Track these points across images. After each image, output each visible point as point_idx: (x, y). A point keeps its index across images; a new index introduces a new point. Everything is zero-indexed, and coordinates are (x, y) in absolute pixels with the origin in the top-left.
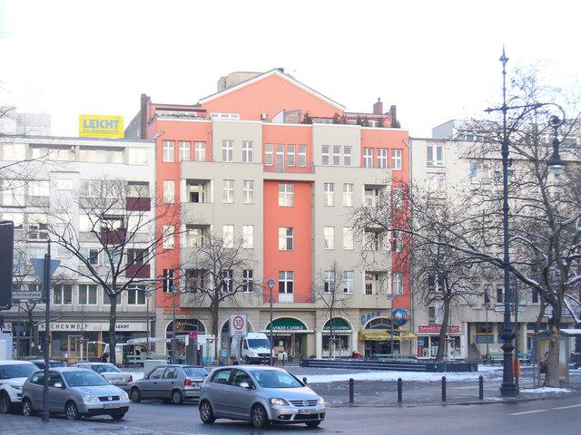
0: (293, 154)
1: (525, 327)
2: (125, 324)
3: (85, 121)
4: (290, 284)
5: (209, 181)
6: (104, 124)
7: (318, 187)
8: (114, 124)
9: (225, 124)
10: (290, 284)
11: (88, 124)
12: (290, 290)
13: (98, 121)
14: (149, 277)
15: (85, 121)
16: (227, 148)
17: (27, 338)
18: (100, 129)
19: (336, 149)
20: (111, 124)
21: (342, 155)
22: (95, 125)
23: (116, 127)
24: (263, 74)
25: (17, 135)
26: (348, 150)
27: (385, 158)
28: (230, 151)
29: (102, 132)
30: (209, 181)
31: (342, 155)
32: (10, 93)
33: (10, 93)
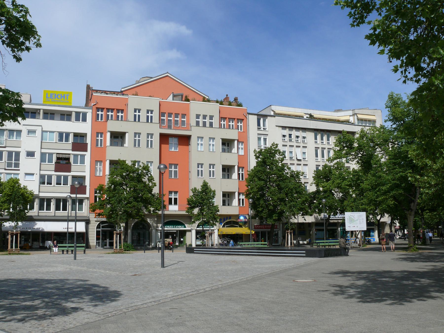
3: (47, 94)
6: (59, 97)
7: (193, 141)
8: (66, 97)
11: (49, 96)
12: (176, 203)
13: (55, 94)
15: (47, 94)
18: (58, 100)
19: (205, 117)
20: (64, 97)
21: (207, 120)
22: (54, 97)
23: (67, 99)
26: (211, 117)
31: (207, 120)
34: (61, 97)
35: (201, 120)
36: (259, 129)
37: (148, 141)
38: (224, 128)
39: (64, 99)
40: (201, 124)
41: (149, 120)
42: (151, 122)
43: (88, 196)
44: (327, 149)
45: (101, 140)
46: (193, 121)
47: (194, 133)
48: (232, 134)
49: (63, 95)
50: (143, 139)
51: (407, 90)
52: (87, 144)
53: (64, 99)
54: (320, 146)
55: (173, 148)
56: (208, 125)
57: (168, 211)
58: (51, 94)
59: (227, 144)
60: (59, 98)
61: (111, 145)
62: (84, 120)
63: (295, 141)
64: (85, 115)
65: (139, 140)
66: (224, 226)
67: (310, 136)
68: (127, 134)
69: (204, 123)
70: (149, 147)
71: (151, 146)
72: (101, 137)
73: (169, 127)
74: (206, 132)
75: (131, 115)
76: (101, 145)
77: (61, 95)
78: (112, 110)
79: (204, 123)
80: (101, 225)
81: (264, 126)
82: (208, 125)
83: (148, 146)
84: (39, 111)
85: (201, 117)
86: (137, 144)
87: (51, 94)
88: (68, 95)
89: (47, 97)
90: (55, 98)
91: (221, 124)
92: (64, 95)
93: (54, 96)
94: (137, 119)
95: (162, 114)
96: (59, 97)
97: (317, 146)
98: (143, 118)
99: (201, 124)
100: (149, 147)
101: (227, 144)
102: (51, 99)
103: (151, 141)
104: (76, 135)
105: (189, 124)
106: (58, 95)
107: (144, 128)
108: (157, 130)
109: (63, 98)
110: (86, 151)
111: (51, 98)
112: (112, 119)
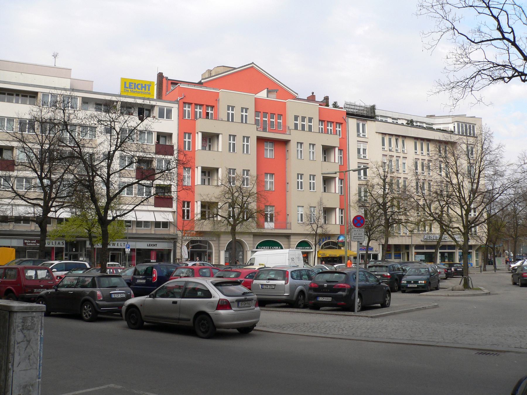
0: (259, 118)
1: (413, 248)
2: (154, 243)
3: (125, 83)
4: (271, 216)
5: (217, 135)
6: (140, 87)
7: (293, 147)
8: (147, 87)
9: (226, 97)
10: (271, 216)
11: (128, 86)
12: (271, 220)
13: (135, 84)
14: (172, 207)
15: (125, 83)
16: (244, 114)
17: (76, 253)
18: (138, 90)
19: (303, 119)
20: (145, 87)
21: (306, 123)
22: (133, 87)
23: (149, 90)
24: (235, 68)
25: (457, 178)
26: (310, 120)
27: (340, 129)
28: (246, 116)
29: (138, 92)
30: (217, 135)
31: (306, 123)
32: (299, 206)
33: (299, 206)
34: (142, 87)
35: (299, 122)
36: (358, 136)
37: (230, 143)
38: (331, 133)
39: (145, 90)
40: (300, 127)
41: (244, 120)
42: (232, 121)
43: (175, 210)
44: (420, 160)
45: (189, 142)
46: (291, 123)
47: (294, 137)
48: (333, 141)
49: (144, 85)
50: (239, 142)
51: (125, 323)
52: (172, 147)
53: (145, 90)
54: (420, 157)
55: (269, 153)
56: (306, 128)
57: (264, 228)
58: (130, 83)
59: (327, 150)
60: (139, 89)
61: (204, 147)
62: (169, 117)
63: (395, 151)
64: (169, 112)
65: (234, 144)
66: (322, 248)
67: (410, 145)
68: (220, 136)
69: (303, 126)
70: (245, 153)
71: (234, 150)
72: (189, 138)
73: (264, 130)
74: (306, 137)
75: (223, 113)
76: (189, 148)
77: (142, 84)
78: (201, 105)
79: (303, 126)
80: (190, 245)
81: (363, 132)
82: (306, 128)
83: (230, 150)
84: (115, 104)
85: (300, 119)
86: (232, 148)
87: (130, 83)
88: (149, 86)
89: (125, 87)
90: (135, 89)
91: (328, 129)
92: (145, 85)
93: (133, 85)
94: (230, 118)
95: (257, 113)
96: (140, 87)
97: (417, 157)
98: (237, 118)
99: (300, 127)
100: (245, 153)
101: (327, 150)
102: (129, 90)
103: (247, 146)
104: (160, 135)
105: (285, 126)
106: (138, 85)
107: (240, 130)
108: (254, 133)
109: (143, 89)
110: (172, 154)
111: (130, 88)
112: (200, 117)
